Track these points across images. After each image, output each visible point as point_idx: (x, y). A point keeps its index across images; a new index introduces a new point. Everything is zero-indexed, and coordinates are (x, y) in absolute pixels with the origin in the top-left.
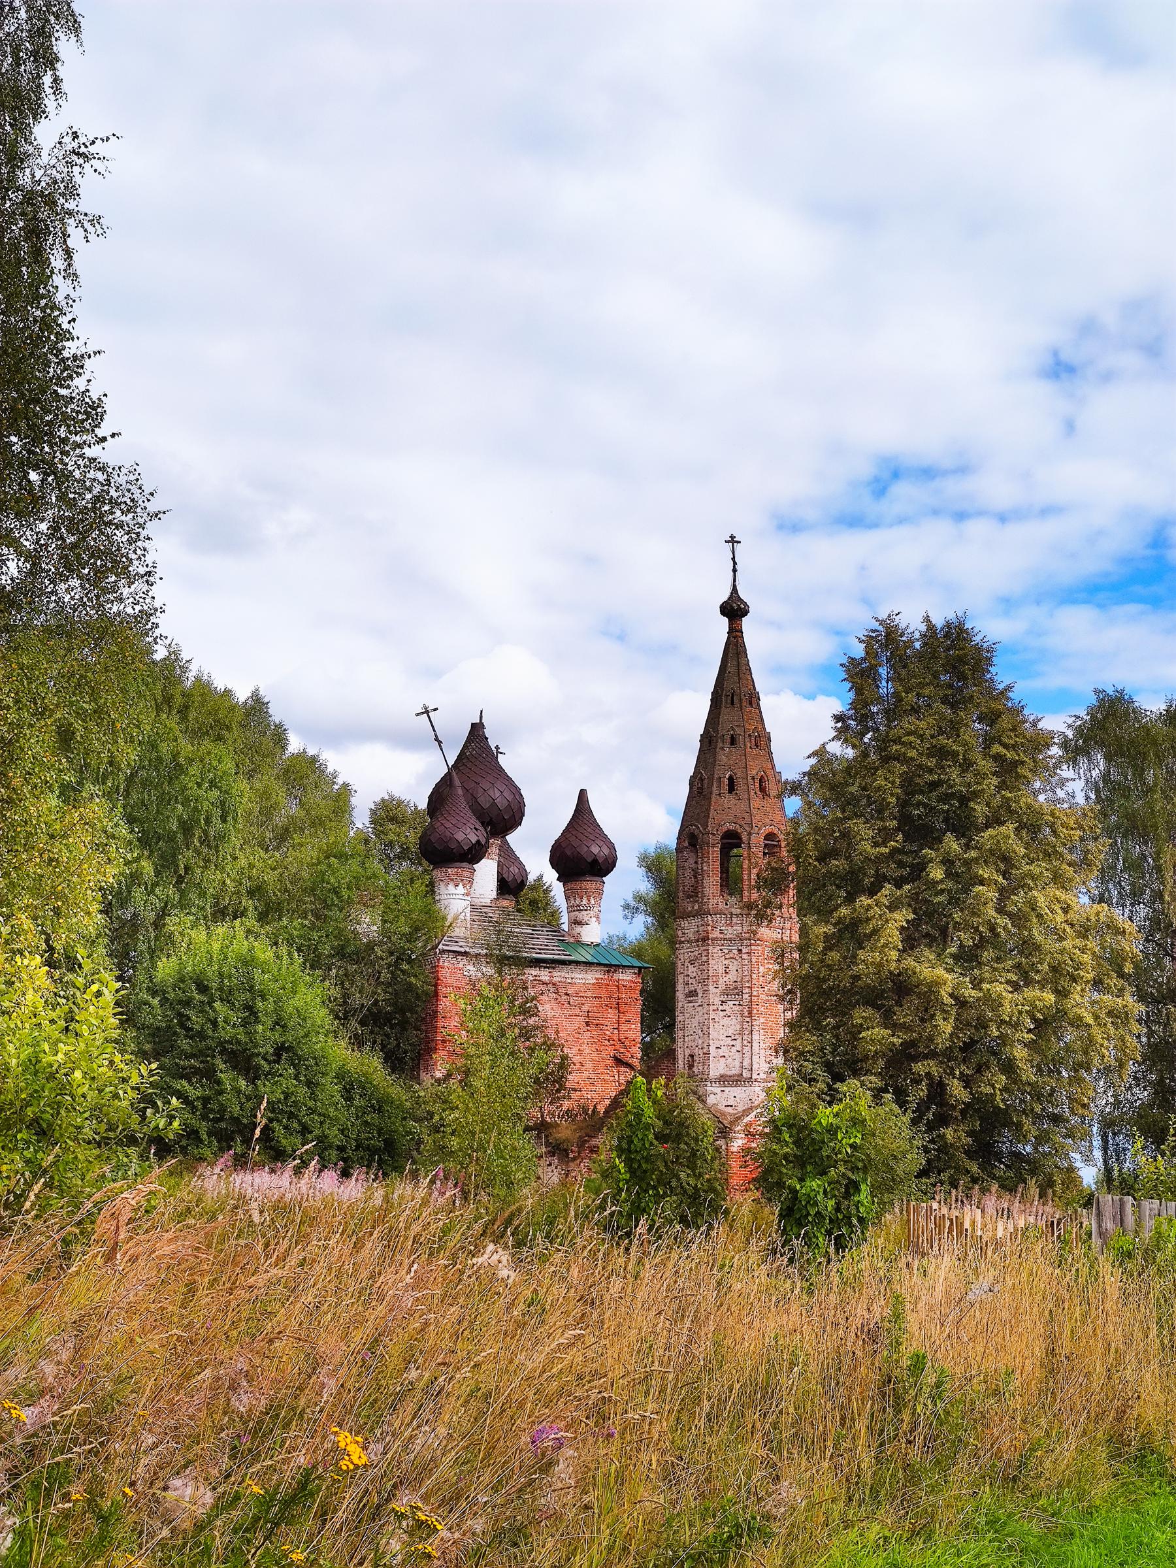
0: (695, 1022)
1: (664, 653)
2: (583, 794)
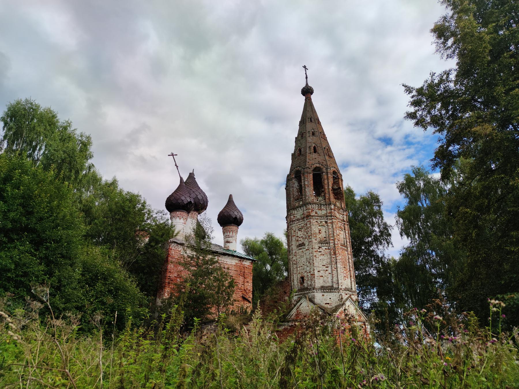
0: (304, 259)
1: (272, 117)
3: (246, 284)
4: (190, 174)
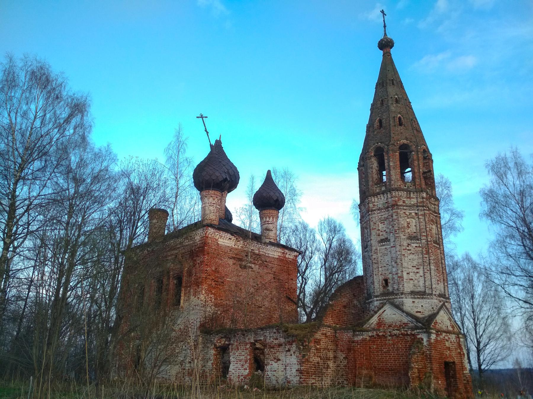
2: (269, 172)
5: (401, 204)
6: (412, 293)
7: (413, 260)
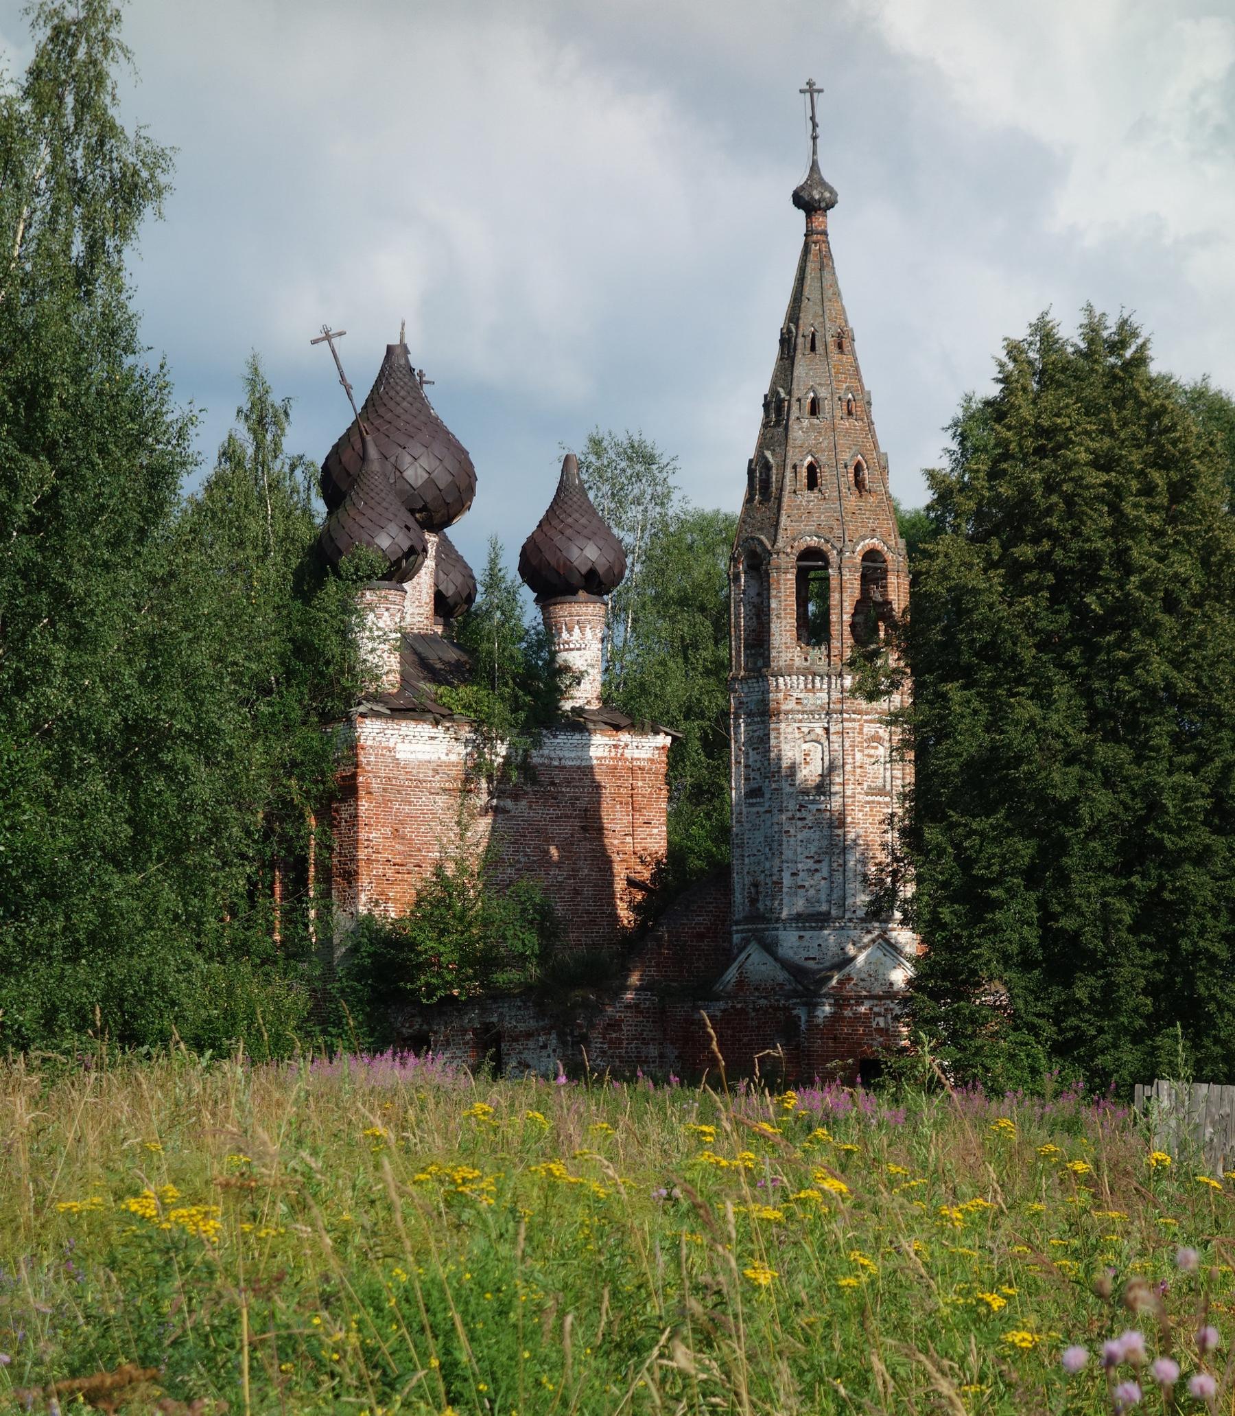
3: (641, 832)
4: (390, 349)
5: (788, 707)
6: (798, 918)
7: (809, 841)
